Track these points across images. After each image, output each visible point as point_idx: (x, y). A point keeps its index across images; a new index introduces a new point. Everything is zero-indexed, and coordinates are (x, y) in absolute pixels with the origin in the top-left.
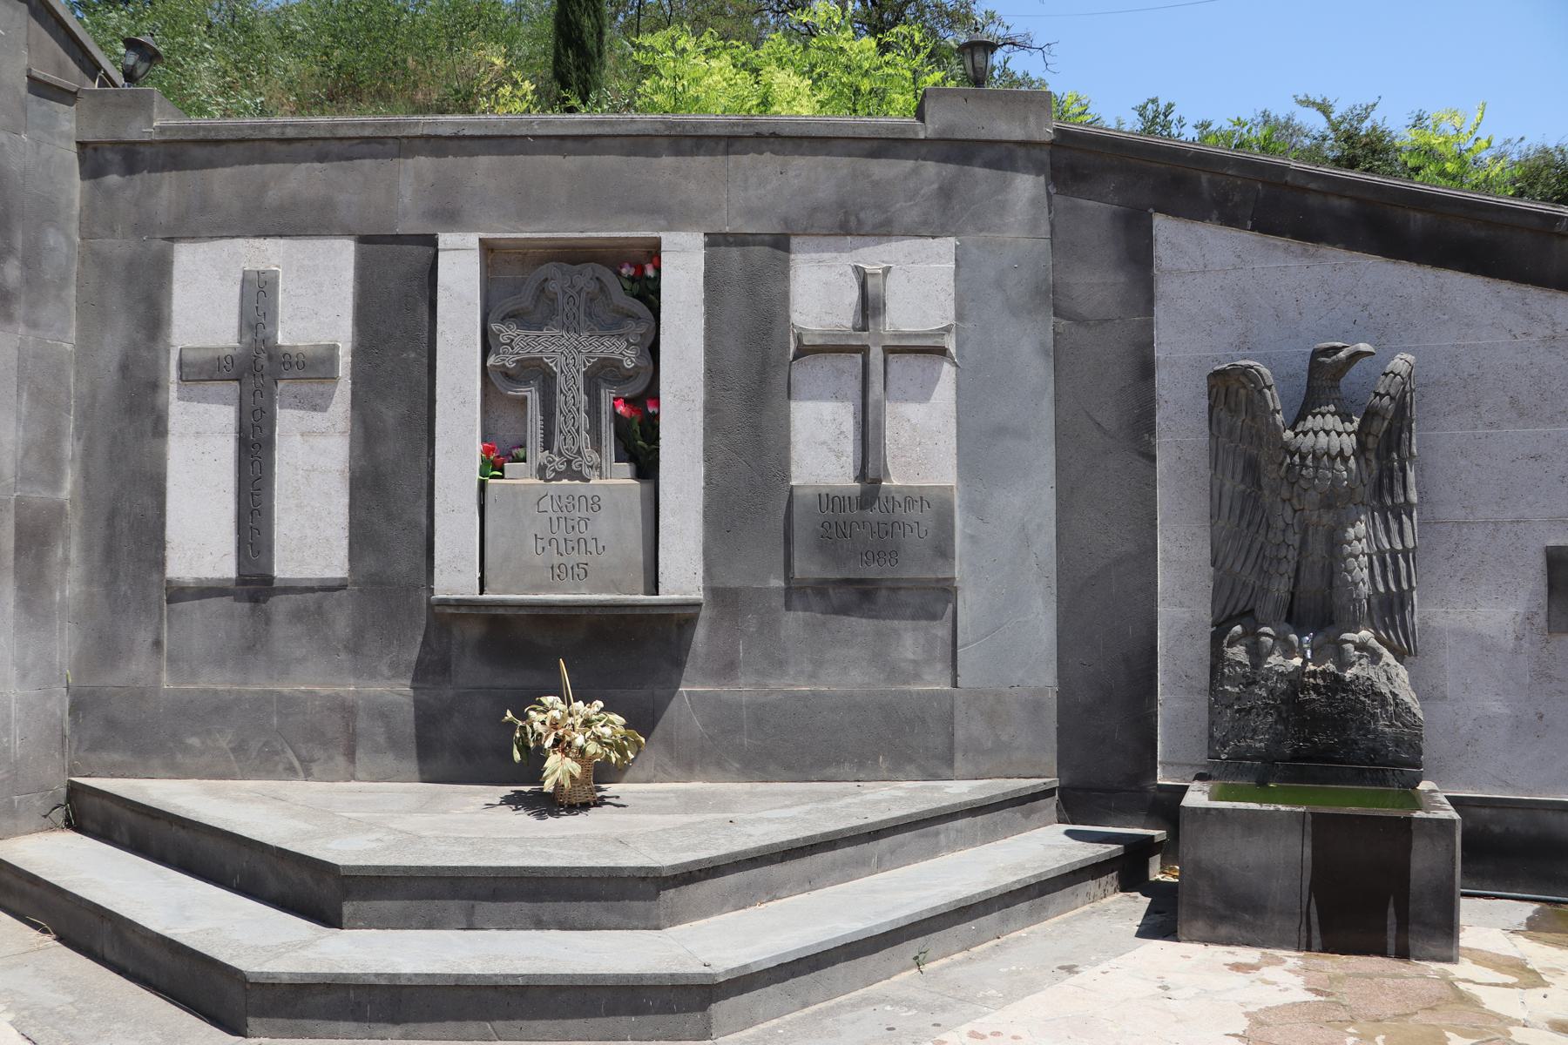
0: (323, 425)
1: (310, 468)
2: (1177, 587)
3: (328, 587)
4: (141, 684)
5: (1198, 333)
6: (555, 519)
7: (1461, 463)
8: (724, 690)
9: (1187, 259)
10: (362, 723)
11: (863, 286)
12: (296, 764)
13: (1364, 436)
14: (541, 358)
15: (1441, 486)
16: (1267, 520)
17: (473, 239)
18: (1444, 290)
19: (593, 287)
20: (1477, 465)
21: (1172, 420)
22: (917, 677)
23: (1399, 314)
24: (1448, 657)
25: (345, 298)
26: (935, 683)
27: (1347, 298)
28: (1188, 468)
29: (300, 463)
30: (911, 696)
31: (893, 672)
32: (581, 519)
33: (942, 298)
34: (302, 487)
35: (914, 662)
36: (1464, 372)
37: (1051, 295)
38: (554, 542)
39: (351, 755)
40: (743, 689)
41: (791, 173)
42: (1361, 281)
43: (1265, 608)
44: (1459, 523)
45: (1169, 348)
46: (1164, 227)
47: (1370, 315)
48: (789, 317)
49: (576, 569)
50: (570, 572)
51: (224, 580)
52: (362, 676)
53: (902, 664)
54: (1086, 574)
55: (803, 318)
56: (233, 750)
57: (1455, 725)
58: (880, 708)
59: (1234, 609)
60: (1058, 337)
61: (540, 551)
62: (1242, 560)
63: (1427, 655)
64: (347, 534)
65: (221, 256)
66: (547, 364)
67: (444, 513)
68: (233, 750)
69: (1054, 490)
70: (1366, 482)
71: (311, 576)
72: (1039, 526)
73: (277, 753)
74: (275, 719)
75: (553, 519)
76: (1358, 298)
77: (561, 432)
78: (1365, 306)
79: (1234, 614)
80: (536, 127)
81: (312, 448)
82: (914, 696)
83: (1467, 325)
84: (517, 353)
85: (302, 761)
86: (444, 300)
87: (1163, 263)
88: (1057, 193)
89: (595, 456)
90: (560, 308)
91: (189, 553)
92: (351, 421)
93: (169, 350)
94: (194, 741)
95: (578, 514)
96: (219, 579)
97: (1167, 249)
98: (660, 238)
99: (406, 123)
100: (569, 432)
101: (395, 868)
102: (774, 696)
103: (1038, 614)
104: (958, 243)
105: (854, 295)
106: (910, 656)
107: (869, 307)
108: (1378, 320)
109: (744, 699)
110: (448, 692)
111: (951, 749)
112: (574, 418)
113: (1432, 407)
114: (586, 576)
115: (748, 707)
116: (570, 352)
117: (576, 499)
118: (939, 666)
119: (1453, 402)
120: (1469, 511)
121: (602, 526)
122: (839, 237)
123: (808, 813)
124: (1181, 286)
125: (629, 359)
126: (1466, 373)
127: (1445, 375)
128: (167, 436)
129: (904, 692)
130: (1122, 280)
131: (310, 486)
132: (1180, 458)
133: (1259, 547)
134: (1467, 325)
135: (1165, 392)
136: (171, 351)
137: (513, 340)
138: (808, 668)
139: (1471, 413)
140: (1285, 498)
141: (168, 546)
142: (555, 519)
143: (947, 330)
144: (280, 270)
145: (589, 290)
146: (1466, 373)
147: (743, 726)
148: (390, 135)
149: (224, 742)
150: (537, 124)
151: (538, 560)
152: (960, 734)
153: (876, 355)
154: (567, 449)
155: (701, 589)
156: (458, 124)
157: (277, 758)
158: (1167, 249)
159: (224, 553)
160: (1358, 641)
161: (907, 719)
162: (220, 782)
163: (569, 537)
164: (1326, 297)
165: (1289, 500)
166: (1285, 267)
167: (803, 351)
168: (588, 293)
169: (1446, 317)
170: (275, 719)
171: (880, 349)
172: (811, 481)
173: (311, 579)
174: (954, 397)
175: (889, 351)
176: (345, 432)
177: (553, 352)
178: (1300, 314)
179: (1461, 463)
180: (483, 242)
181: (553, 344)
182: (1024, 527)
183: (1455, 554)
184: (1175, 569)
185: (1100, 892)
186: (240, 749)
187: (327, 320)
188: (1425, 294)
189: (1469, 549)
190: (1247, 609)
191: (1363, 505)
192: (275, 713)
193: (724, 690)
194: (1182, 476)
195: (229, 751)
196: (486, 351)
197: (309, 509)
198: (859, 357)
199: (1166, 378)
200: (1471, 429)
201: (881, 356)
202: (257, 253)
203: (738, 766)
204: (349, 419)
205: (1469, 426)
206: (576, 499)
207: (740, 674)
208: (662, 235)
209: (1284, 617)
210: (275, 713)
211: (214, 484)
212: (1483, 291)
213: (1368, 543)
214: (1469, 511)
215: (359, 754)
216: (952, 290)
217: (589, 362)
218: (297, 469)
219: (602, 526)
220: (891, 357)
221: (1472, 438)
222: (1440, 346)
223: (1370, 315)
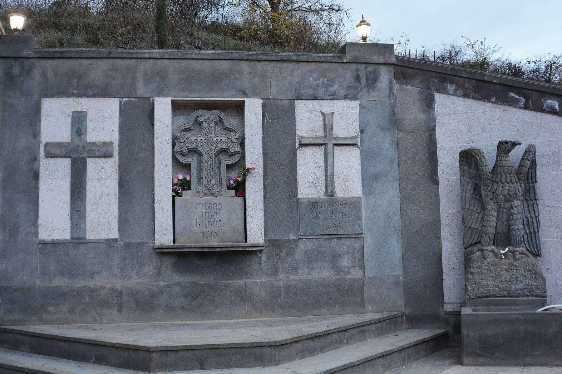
0: (107, 175)
1: (101, 193)
2: (449, 234)
3: (110, 242)
4: (28, 285)
5: (453, 137)
6: (204, 213)
7: (553, 184)
8: (274, 280)
9: (448, 109)
10: (125, 299)
11: (324, 119)
12: (97, 316)
13: (519, 174)
14: (197, 148)
15: (546, 193)
16: (484, 207)
17: (169, 100)
18: (544, 120)
19: (218, 119)
20: (559, 185)
21: (444, 171)
22: (349, 273)
23: (528, 129)
24: (552, 257)
25: (115, 123)
26: (356, 274)
27: (509, 123)
28: (451, 189)
29: (97, 191)
30: (347, 280)
31: (339, 271)
32: (215, 213)
33: (354, 124)
34: (98, 201)
35: (348, 267)
36: (553, 150)
37: (396, 123)
38: (204, 222)
39: (120, 310)
40: (282, 279)
41: (295, 75)
42: (514, 117)
43: (485, 239)
44: (554, 207)
45: (442, 143)
46: (438, 98)
47: (518, 129)
48: (296, 132)
49: (213, 233)
50: (210, 234)
51: (64, 240)
52: (124, 279)
53: (343, 268)
54: (413, 231)
55: (301, 132)
56: (69, 312)
57: (556, 282)
58: (335, 286)
59: (472, 242)
60: (399, 139)
61: (198, 226)
62: (475, 223)
63: (544, 257)
64: (117, 220)
65: (62, 105)
66: (199, 150)
67: (159, 211)
68: (69, 312)
69: (399, 198)
70: (520, 192)
71: (102, 238)
72: (394, 213)
73: (88, 312)
74: (87, 298)
75: (203, 213)
76: (513, 123)
77: (206, 178)
78: (516, 126)
79: (472, 243)
80: (194, 55)
81: (102, 185)
82: (348, 281)
83: (553, 133)
84: (187, 146)
85: (99, 316)
86: (157, 124)
87: (439, 111)
88: (397, 84)
89: (219, 187)
90: (204, 128)
91: (49, 229)
92: (118, 174)
93: (39, 144)
94: (51, 309)
95: (213, 211)
96: (62, 240)
97: (440, 105)
98: (244, 101)
99: (140, 52)
100: (209, 178)
101: (109, 343)
102: (293, 282)
103: (395, 247)
104: (360, 103)
105: (321, 124)
106: (346, 265)
107: (327, 127)
108: (521, 131)
109: (282, 284)
110: (162, 284)
111: (363, 301)
112: (210, 172)
113: (542, 164)
114: (217, 236)
115: (283, 287)
116: (208, 146)
117: (212, 204)
118: (357, 269)
119: (549, 162)
120: (557, 202)
121: (223, 216)
122: (314, 101)
123: (20, 322)
124: (446, 119)
125: (234, 148)
126: (553, 151)
127: (546, 151)
128: (39, 180)
129: (344, 279)
130: (424, 117)
131: (101, 201)
132: (448, 185)
133: (481, 217)
134: (553, 133)
135: (441, 160)
136: (41, 144)
137: (185, 141)
138: (307, 270)
139: (556, 166)
140: (491, 198)
141: (40, 226)
142: (204, 213)
143: (357, 137)
144: (88, 111)
145: (215, 121)
146: (553, 151)
147: (281, 295)
148: (133, 57)
149: (65, 308)
150: (194, 54)
151: (197, 230)
152: (366, 295)
153: (330, 145)
154: (208, 185)
155: (264, 240)
156: (162, 53)
157: (88, 315)
158: (440, 105)
159: (64, 229)
160: (520, 251)
161: (346, 289)
162: (444, 265)
163: (210, 220)
164: (501, 123)
165: (492, 199)
166: (486, 112)
167: (302, 145)
168: (215, 122)
169: (545, 130)
170: (87, 298)
171: (331, 145)
172: (306, 196)
173: (102, 239)
174: (360, 163)
175: (335, 145)
176: (116, 178)
177: (202, 146)
178: (492, 129)
179: (553, 184)
180: (172, 101)
181: (201, 142)
182: (388, 213)
183: (553, 219)
184: (448, 228)
185: (393, 350)
186: (72, 311)
187: (108, 132)
188: (538, 121)
189: (558, 216)
190: (477, 242)
191: (520, 200)
192: (87, 296)
193: (274, 280)
194: (449, 192)
195: (67, 312)
196: (174, 145)
197: (101, 210)
198: (323, 148)
199: (441, 154)
200: (556, 171)
201: (332, 148)
202: (77, 104)
203: (280, 311)
204: (118, 173)
205: (556, 171)
206: (212, 204)
207: (280, 274)
208: (245, 99)
209: (492, 243)
210: (87, 296)
211: (59, 200)
212: (558, 120)
213: (522, 215)
214: (557, 202)
215: (124, 311)
216: (358, 121)
217: (216, 149)
218: (96, 193)
219: (223, 216)
220: (335, 147)
221: (557, 175)
222: (544, 141)
223: (518, 129)
